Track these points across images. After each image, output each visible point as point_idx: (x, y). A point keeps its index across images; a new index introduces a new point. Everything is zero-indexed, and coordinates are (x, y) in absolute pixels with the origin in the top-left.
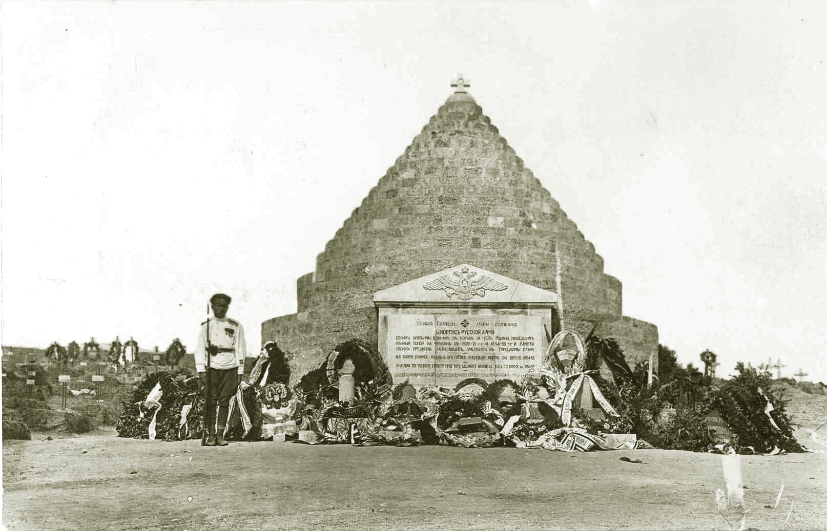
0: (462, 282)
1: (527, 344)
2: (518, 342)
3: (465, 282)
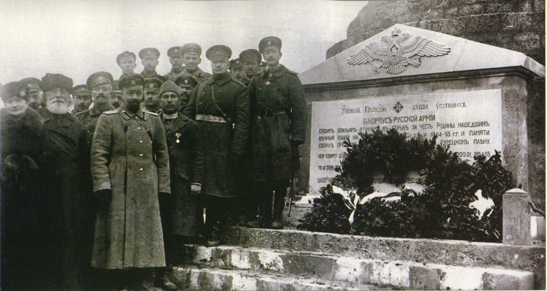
0: (391, 50)
1: (480, 132)
2: (467, 130)
3: (394, 50)
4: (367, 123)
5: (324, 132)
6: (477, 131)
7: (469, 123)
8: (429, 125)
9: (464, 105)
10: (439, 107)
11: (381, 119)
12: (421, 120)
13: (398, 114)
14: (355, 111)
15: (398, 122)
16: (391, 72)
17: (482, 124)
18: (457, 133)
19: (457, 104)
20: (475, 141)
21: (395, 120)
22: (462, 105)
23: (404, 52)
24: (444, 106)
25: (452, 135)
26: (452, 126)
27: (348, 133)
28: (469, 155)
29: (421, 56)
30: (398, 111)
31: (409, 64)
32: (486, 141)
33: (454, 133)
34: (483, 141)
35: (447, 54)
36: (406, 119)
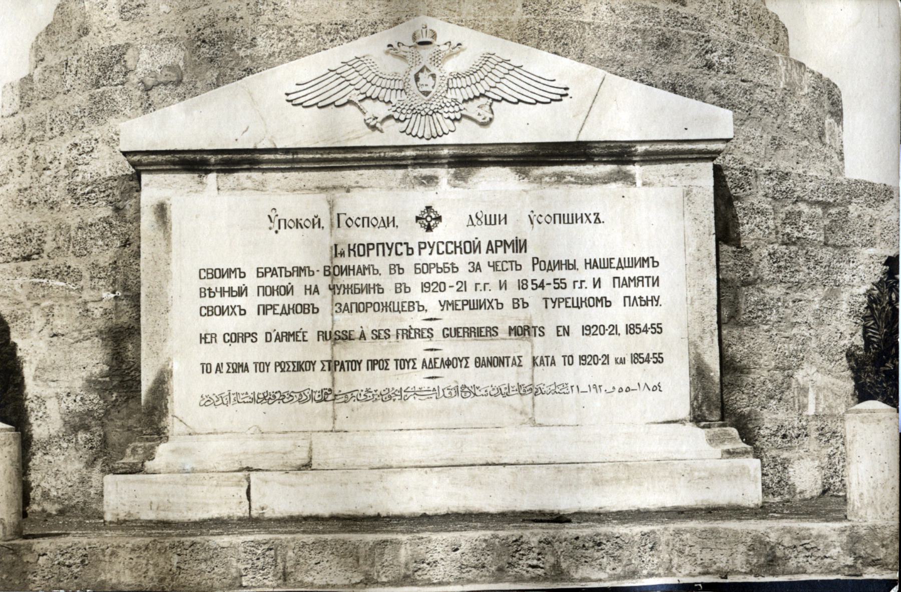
0: (417, 79)
1: (637, 281)
2: (606, 276)
4: (342, 254)
5: (214, 276)
6: (629, 278)
7: (611, 259)
8: (511, 262)
9: (597, 218)
10: (535, 222)
11: (383, 244)
12: (492, 250)
13: (429, 233)
14: (307, 223)
15: (430, 254)
16: (414, 133)
17: (643, 261)
18: (582, 281)
19: (579, 216)
20: (627, 299)
21: (420, 248)
22: (592, 218)
23: (451, 86)
24: (548, 219)
25: (570, 285)
26: (570, 266)
27: (291, 279)
28: (614, 332)
29: (494, 100)
30: (429, 229)
31: (462, 116)
32: (652, 300)
33: (476, 284)
34: (645, 299)
35: (561, 100)
36: (451, 248)
